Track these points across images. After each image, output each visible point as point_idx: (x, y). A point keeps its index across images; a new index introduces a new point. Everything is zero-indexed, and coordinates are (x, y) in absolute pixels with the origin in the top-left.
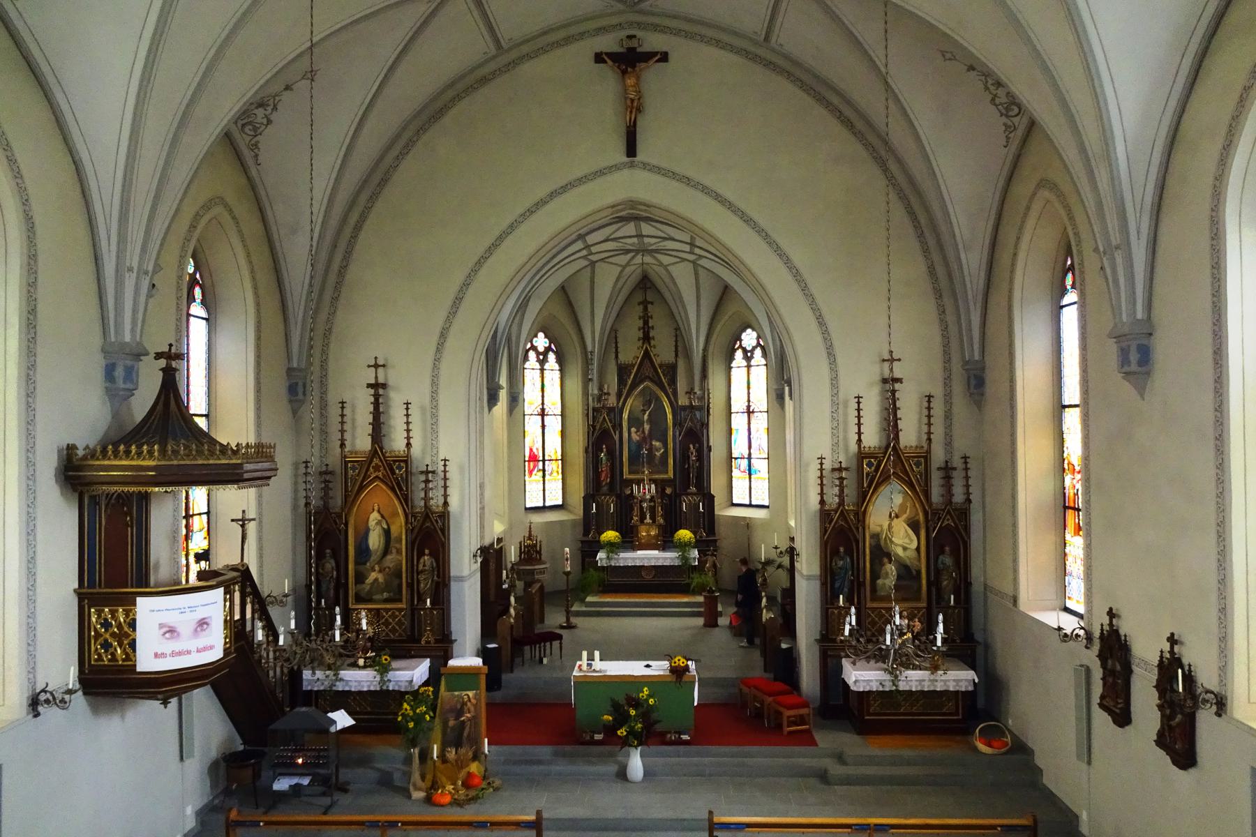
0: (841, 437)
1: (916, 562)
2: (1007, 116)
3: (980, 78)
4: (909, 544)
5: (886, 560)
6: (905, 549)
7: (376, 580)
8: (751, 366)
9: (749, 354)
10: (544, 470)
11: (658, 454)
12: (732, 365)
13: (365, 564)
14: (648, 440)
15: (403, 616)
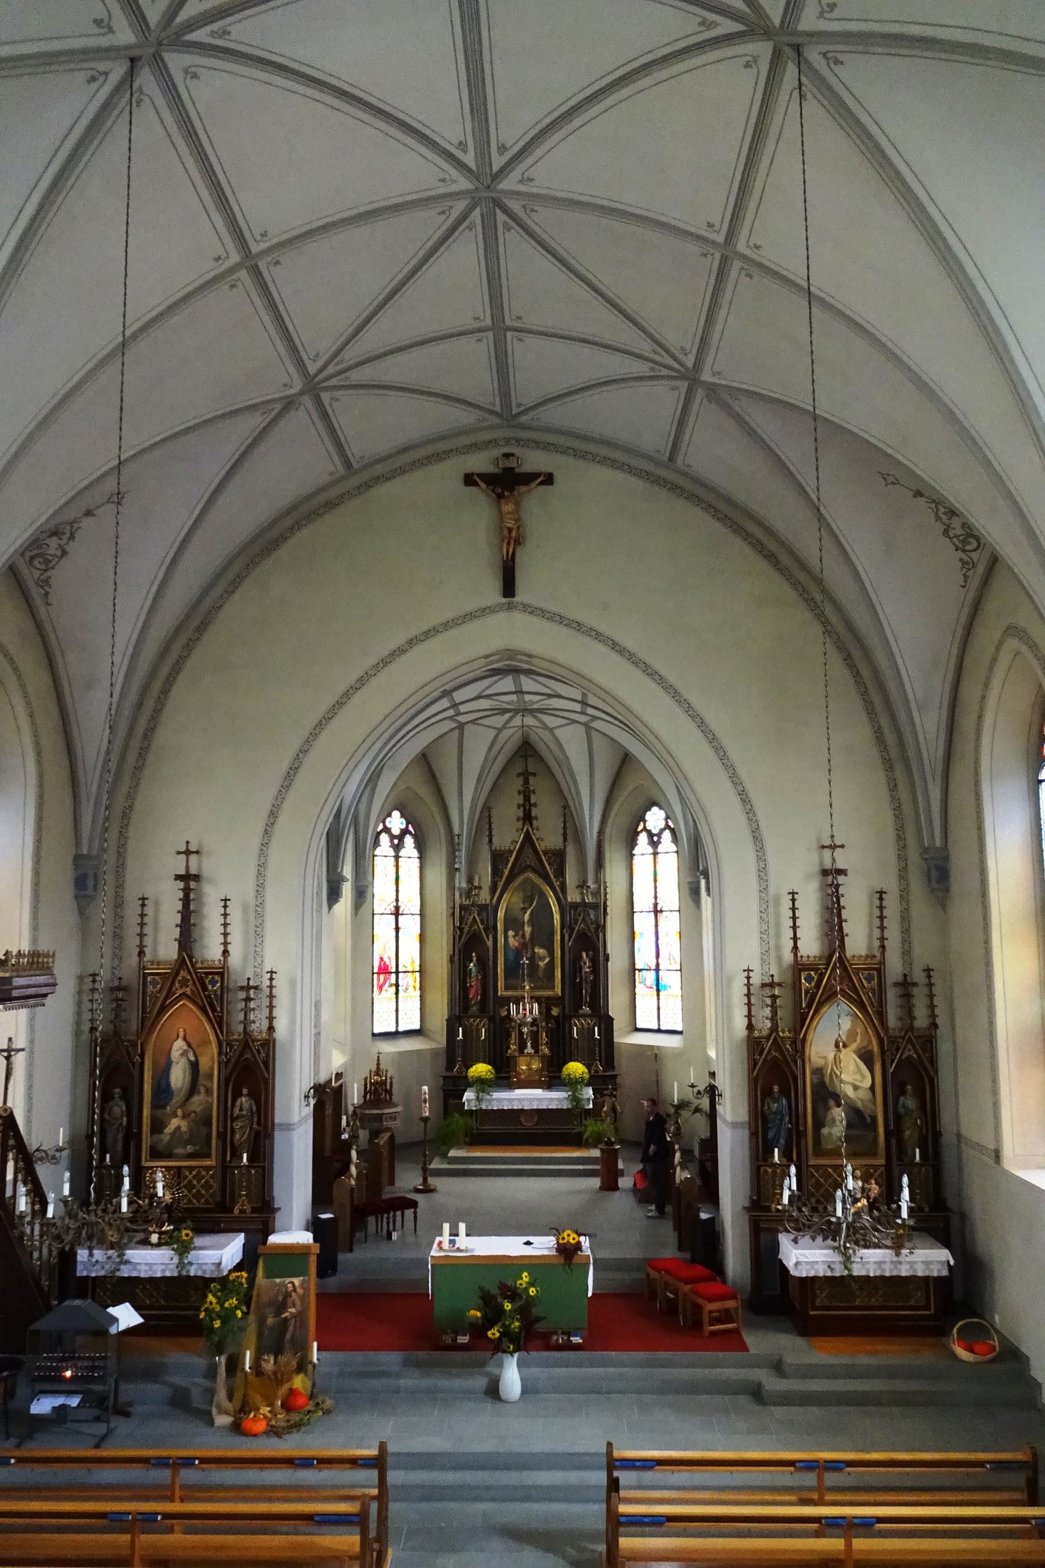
0: (772, 943)
1: (872, 1106)
2: (964, 551)
3: (930, 505)
4: (861, 1081)
5: (832, 1102)
6: (856, 1088)
7: (178, 1128)
8: (658, 853)
9: (655, 839)
10: (397, 985)
11: (541, 964)
12: (634, 852)
13: (164, 1107)
14: (529, 947)
15: (211, 1177)
